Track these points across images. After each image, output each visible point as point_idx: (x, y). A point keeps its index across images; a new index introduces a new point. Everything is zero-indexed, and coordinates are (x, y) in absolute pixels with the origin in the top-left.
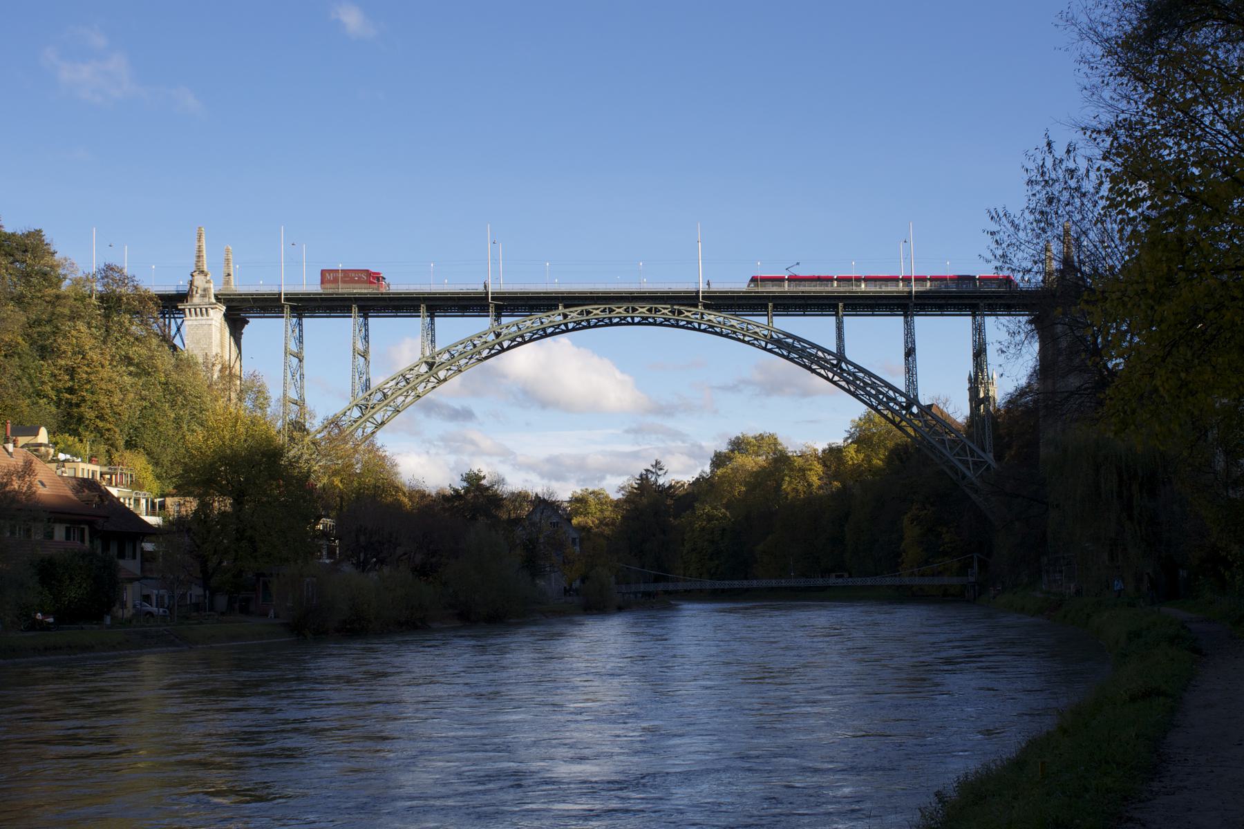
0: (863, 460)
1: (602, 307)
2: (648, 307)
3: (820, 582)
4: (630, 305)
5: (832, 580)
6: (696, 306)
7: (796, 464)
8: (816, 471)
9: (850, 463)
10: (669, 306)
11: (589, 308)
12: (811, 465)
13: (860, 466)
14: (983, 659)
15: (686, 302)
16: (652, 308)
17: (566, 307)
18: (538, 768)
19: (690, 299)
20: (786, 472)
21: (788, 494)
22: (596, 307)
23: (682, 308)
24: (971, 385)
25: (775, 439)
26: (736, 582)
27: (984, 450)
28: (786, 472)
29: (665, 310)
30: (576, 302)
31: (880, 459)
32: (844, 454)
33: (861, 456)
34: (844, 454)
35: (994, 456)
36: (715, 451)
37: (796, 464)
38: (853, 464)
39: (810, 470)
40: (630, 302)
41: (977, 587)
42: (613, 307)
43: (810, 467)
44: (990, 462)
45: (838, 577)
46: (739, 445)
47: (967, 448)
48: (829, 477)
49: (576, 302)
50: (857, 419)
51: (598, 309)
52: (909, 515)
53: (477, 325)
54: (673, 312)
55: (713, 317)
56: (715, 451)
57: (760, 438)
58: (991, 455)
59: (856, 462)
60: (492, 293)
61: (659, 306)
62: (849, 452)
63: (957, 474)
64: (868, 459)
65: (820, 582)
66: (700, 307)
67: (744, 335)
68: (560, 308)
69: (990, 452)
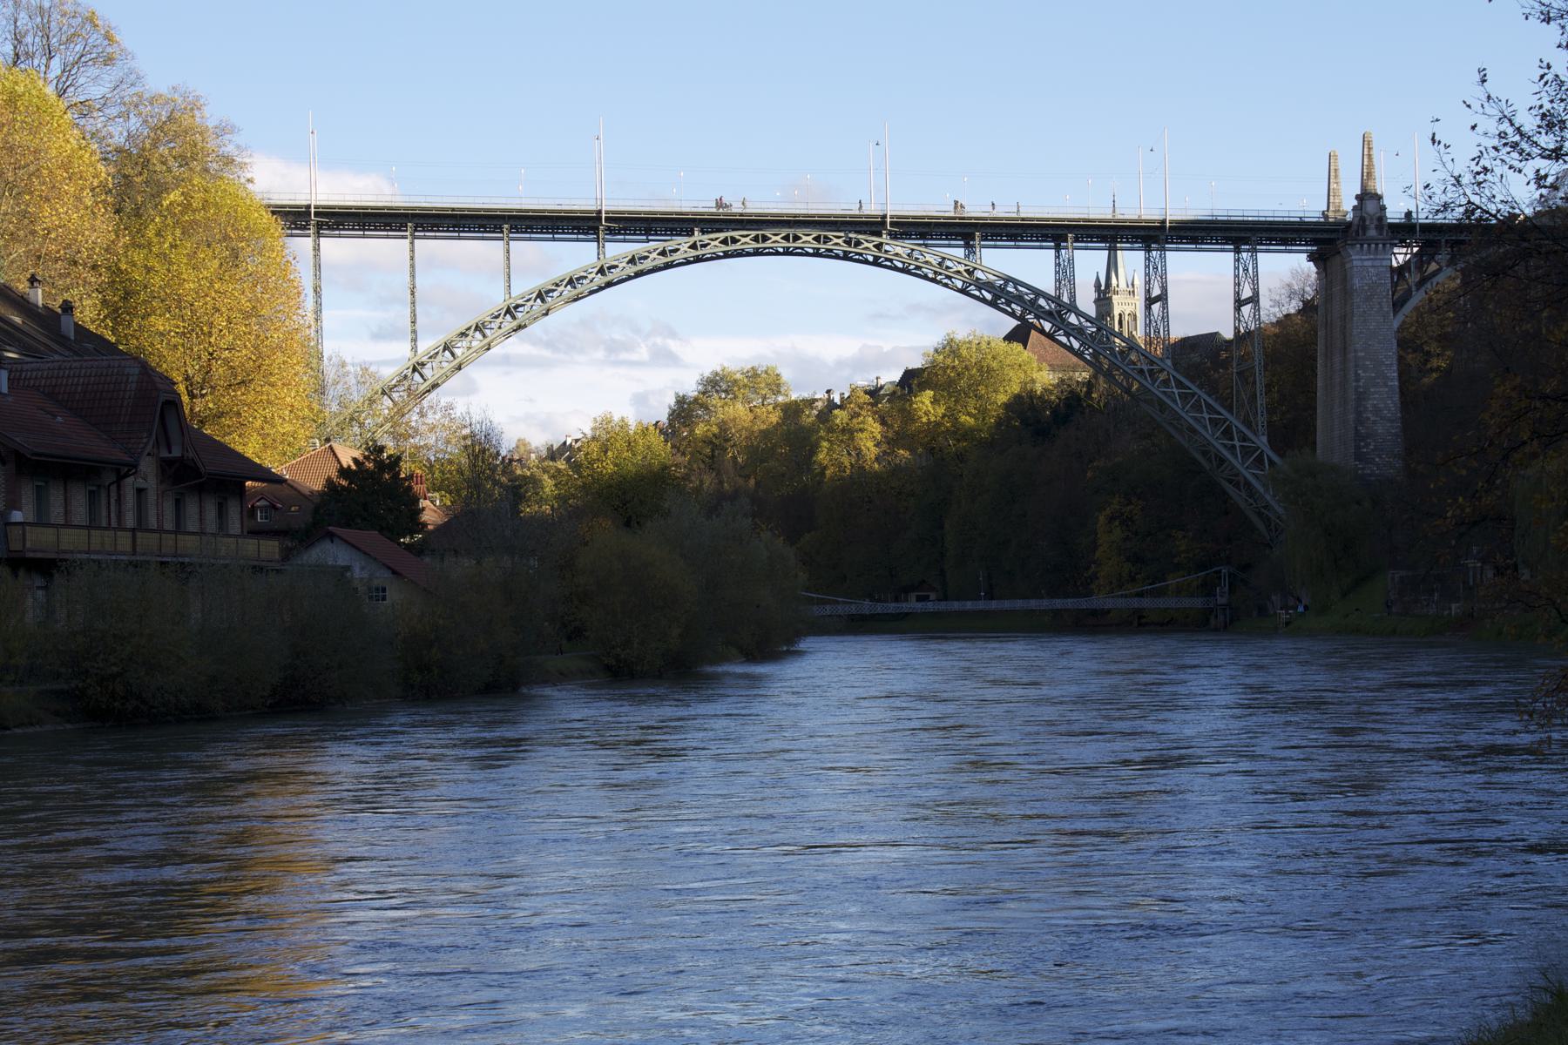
0: (944, 416)
1: (753, 233)
2: (815, 234)
3: (892, 607)
4: (791, 232)
5: (912, 605)
6: (879, 234)
7: (838, 421)
8: (872, 433)
9: (924, 420)
10: (842, 234)
11: (736, 234)
12: (863, 422)
13: (938, 424)
14: (1246, 702)
15: (865, 228)
16: (820, 236)
18: (923, 799)
19: (874, 226)
20: (822, 433)
21: (825, 468)
22: (745, 233)
23: (860, 237)
24: (1099, 295)
25: (778, 375)
26: (1058, 601)
27: (1255, 433)
28: (822, 433)
29: (837, 241)
31: (969, 414)
32: (915, 406)
33: (941, 410)
34: (915, 406)
35: (1269, 441)
36: (677, 394)
37: (838, 421)
38: (929, 422)
39: (862, 430)
40: (790, 228)
41: (1228, 612)
42: (768, 233)
43: (862, 426)
44: (1263, 448)
45: (919, 599)
46: (715, 384)
47: (1234, 429)
48: (888, 442)
49: (717, 226)
50: (932, 351)
52: (1108, 511)
53: (577, 255)
54: (848, 242)
55: (898, 248)
56: (677, 394)
57: (753, 375)
58: (1264, 439)
59: (933, 419)
60: (607, 212)
61: (830, 234)
62: (923, 403)
63: (1209, 460)
64: (951, 414)
65: (892, 607)
66: (884, 236)
67: (935, 273)
68: (696, 233)
69: (1263, 434)
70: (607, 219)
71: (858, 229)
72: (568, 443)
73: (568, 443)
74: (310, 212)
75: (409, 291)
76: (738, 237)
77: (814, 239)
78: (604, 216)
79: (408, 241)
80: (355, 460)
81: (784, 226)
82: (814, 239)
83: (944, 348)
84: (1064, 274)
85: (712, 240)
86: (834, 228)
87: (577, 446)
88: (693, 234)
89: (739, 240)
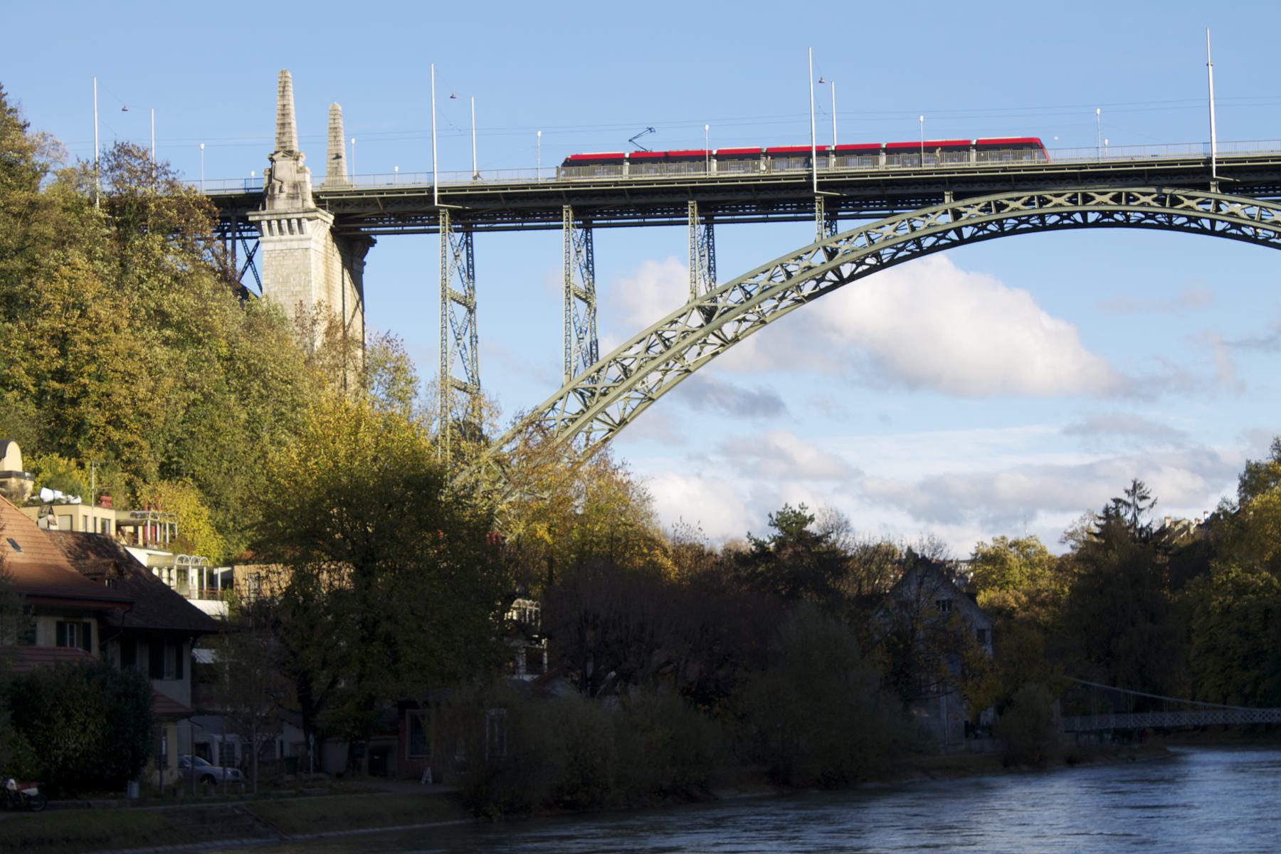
2: (1113, 192)
6: (1206, 188)
10: (1153, 190)
15: (1186, 180)
16: (1120, 194)
17: (957, 197)
22: (1015, 195)
23: (1177, 192)
29: (1146, 198)
30: (976, 188)
40: (1079, 184)
42: (1046, 194)
49: (976, 188)
51: (1018, 199)
55: (1239, 207)
66: (1213, 189)
68: (947, 199)
70: (1220, 171)
71: (1176, 181)
72: (1167, 526)
73: (1167, 526)
74: (1211, 169)
75: (441, 299)
76: (1005, 202)
77: (1112, 199)
78: (1214, 166)
79: (688, 227)
80: (213, 660)
81: (1069, 183)
82: (1112, 199)
83: (1182, 845)
84: (225, 771)
85: (968, 206)
86: (1141, 182)
87: (1176, 529)
88: (943, 201)
89: (1007, 206)
